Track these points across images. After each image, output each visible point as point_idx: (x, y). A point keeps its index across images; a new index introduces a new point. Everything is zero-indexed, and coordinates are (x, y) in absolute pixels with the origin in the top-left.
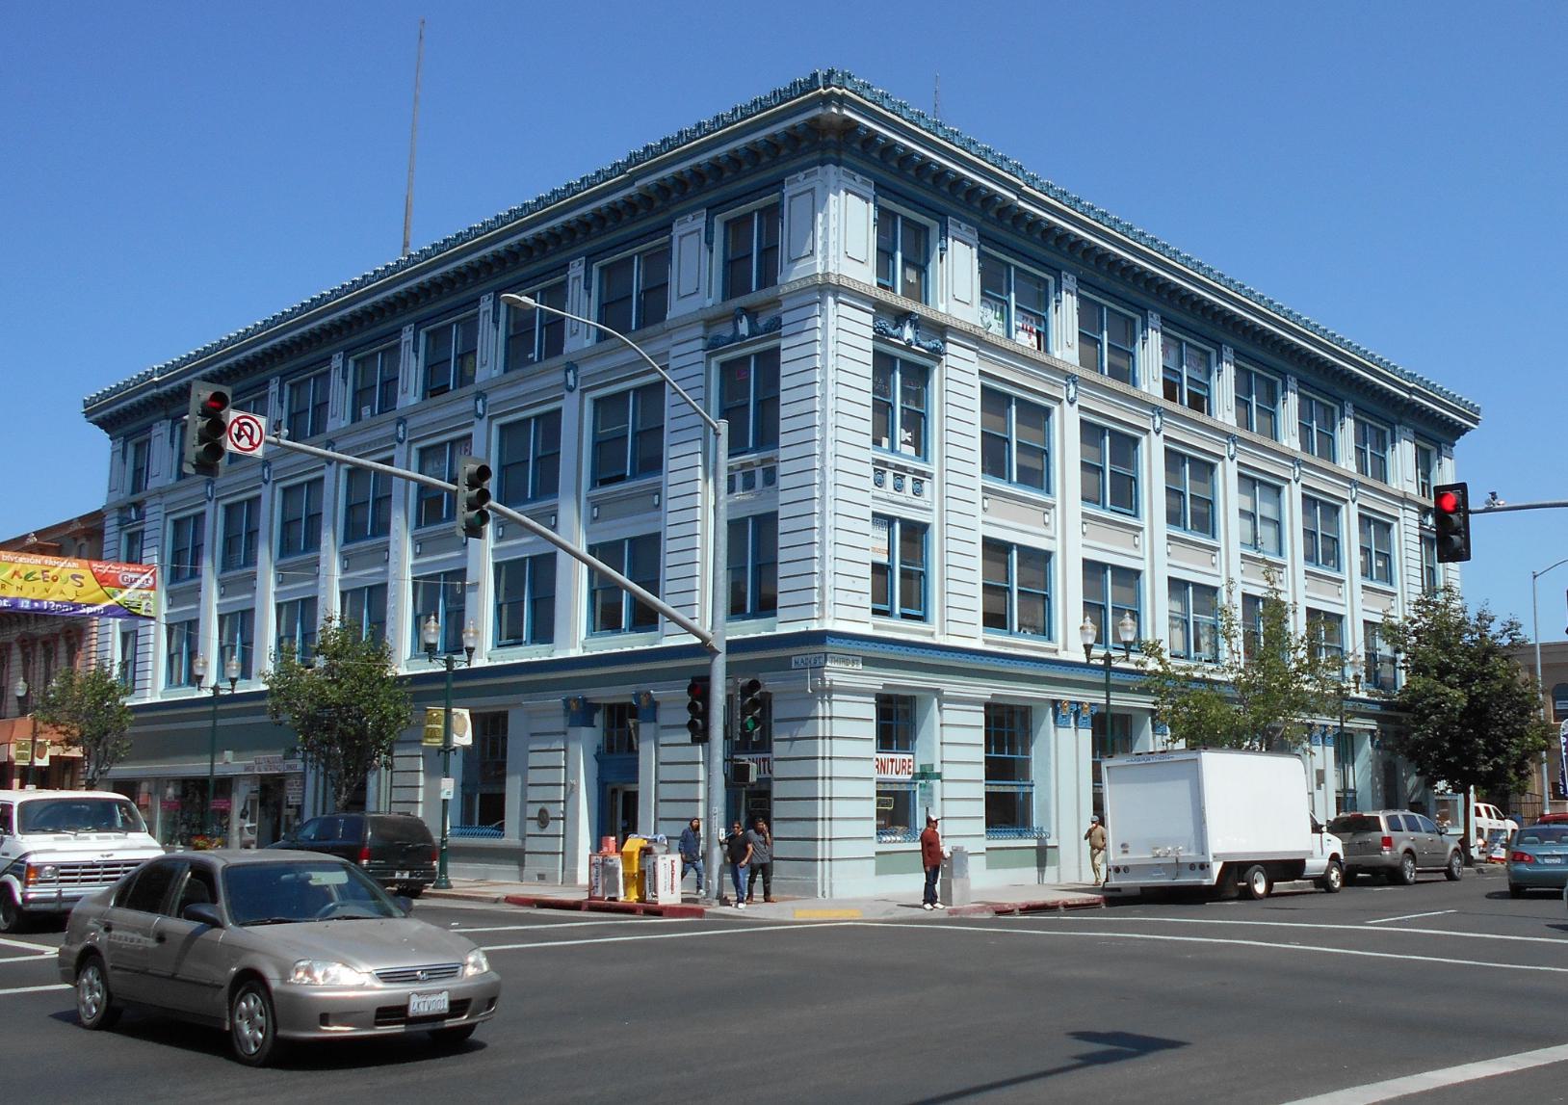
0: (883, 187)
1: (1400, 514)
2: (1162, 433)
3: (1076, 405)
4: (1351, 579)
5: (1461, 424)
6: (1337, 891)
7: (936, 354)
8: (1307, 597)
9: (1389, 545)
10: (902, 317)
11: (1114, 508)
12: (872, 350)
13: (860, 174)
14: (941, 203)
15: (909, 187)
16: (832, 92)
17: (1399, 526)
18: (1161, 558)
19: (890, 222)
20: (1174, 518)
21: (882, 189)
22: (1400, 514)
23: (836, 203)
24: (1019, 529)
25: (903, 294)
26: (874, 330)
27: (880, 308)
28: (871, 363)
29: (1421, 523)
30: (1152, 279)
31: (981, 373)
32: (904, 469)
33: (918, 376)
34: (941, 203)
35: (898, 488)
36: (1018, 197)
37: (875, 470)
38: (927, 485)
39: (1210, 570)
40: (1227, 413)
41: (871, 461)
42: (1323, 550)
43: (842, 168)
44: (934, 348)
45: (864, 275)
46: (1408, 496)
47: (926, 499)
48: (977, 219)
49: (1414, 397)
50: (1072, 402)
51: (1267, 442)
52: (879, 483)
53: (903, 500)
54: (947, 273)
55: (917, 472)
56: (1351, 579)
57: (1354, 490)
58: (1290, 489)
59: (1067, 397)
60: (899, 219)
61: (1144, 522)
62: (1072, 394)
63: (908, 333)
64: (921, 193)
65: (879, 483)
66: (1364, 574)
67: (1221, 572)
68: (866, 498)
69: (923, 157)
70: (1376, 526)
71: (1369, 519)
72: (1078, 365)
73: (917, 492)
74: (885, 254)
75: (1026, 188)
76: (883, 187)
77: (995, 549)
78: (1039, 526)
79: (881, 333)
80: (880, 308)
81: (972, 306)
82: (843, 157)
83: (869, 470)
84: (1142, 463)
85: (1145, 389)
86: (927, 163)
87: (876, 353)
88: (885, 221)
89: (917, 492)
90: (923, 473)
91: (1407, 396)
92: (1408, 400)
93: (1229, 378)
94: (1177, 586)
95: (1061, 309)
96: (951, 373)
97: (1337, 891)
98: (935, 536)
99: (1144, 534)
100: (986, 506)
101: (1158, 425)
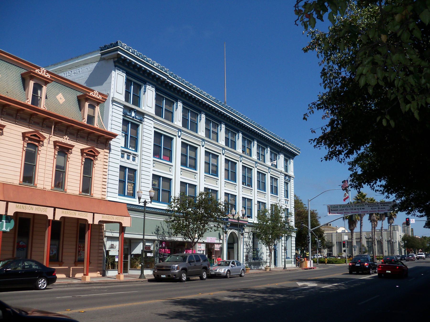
0: (158, 89)
1: (280, 176)
2: (204, 146)
3: (204, 147)
4: (239, 185)
5: (295, 153)
6: (204, 279)
7: (141, 121)
8: (258, 198)
9: (137, 134)
10: (131, 110)
11: (212, 174)
12: (122, 119)
13: (122, 69)
14: (200, 108)
15: (191, 103)
16: (118, 47)
17: (280, 179)
18: (241, 193)
19: (130, 83)
20: (184, 164)
21: (127, 74)
22: (280, 176)
23: (114, 77)
24: (163, 172)
25: (132, 104)
26: (123, 113)
27: (125, 107)
28: (122, 123)
29: (285, 178)
30: (197, 100)
31: (154, 127)
32: (130, 153)
33: (136, 127)
34: (200, 108)
35: (128, 158)
36: (167, 78)
37: (121, 153)
38: (137, 158)
39: (251, 195)
40: (178, 122)
41: (120, 151)
42: (262, 186)
43: (116, 67)
44: (140, 120)
45: (121, 98)
46: (282, 172)
47: (125, 159)
48: (155, 84)
49: (284, 146)
50: (223, 154)
51: (262, 163)
52: (123, 157)
53: (124, 161)
54: (145, 99)
55: (134, 154)
56: (239, 185)
57: (241, 158)
58: (254, 169)
59: (178, 135)
60: (133, 82)
61: (267, 193)
62: (179, 134)
63: (133, 114)
64: (166, 90)
65: (123, 157)
66: (243, 184)
67: (219, 186)
68: (118, 162)
69: (176, 86)
70: (274, 179)
71: (229, 161)
72: (124, 101)
73: (134, 160)
74: (127, 93)
75: (170, 76)
76: (158, 89)
77: (123, 168)
78: (264, 198)
79: (125, 114)
80: (125, 107)
81: (152, 108)
82: (282, 151)
83: (120, 154)
84: (174, 147)
85: (143, 108)
86: (155, 75)
87: (123, 120)
88: (128, 83)
89: (134, 160)
90: (135, 155)
91: (283, 145)
92: (283, 146)
93: (180, 112)
94: (244, 199)
95: (146, 94)
96: (145, 127)
97: (204, 279)
98: (138, 173)
99: (173, 168)
100: (154, 166)
101: (179, 134)
